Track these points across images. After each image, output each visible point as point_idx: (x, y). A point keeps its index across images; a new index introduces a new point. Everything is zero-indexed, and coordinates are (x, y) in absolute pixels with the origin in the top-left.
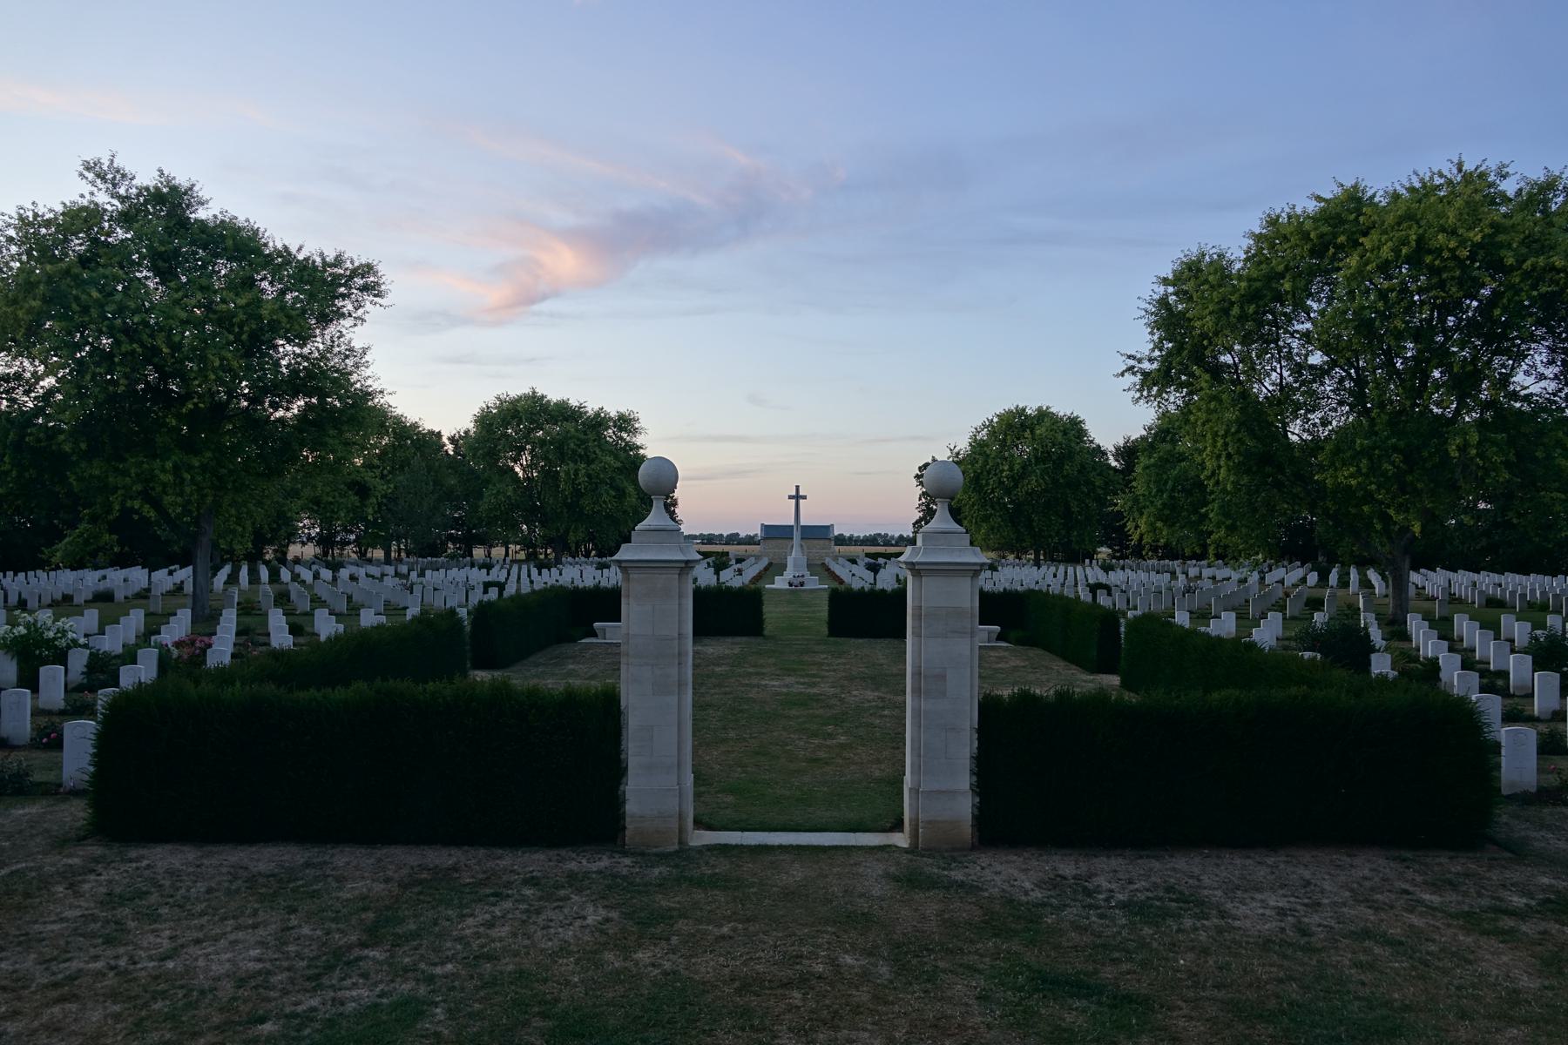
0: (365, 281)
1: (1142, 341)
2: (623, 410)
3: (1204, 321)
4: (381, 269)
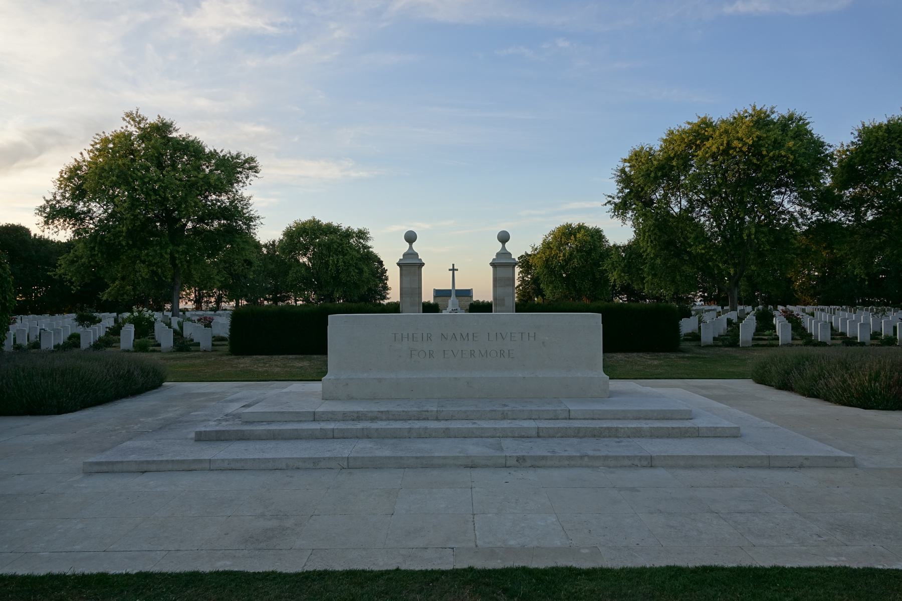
0: (250, 165)
1: (613, 188)
2: (361, 228)
3: (643, 181)
4: (258, 159)
